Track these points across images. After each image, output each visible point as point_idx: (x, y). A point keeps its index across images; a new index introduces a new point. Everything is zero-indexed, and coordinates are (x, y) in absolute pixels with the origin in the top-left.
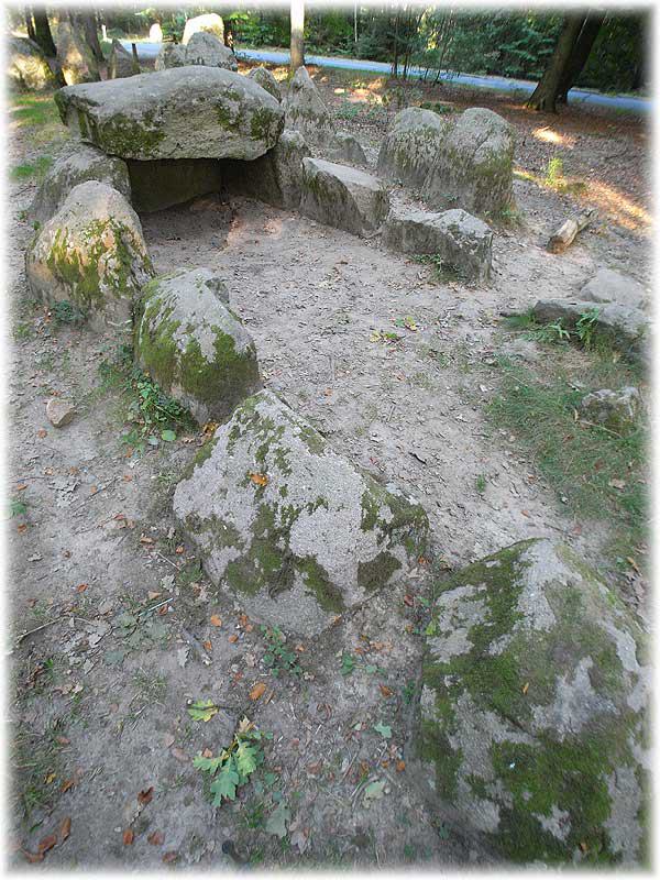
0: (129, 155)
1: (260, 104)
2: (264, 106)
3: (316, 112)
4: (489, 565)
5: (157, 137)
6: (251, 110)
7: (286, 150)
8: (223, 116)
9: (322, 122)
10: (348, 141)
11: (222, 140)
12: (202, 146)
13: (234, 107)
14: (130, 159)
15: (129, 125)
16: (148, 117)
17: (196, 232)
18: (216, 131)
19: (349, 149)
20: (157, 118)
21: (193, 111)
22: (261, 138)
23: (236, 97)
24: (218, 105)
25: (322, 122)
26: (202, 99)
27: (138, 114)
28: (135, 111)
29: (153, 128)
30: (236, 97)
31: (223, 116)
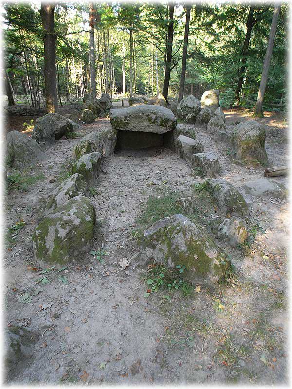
0: (118, 128)
1: (164, 116)
2: (166, 117)
3: (220, 124)
4: (49, 147)
5: (127, 124)
6: (160, 118)
7: (178, 132)
8: (150, 119)
9: (221, 128)
10: (223, 134)
11: (149, 126)
12: (142, 128)
13: (154, 116)
14: (118, 130)
15: (119, 120)
16: (125, 118)
17: (4, 92)
18: (148, 123)
19: (222, 138)
20: (128, 119)
21: (140, 117)
22: (164, 127)
23: (155, 114)
24: (148, 116)
25: (221, 128)
26: (143, 114)
27: (122, 117)
28: (122, 116)
29: (126, 121)
30: (155, 114)
31: (150, 119)
